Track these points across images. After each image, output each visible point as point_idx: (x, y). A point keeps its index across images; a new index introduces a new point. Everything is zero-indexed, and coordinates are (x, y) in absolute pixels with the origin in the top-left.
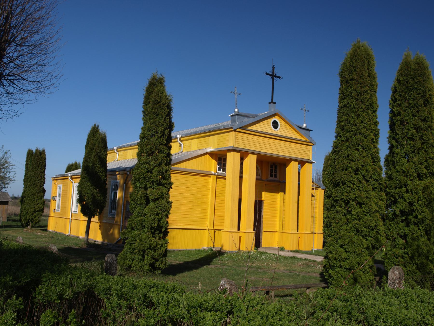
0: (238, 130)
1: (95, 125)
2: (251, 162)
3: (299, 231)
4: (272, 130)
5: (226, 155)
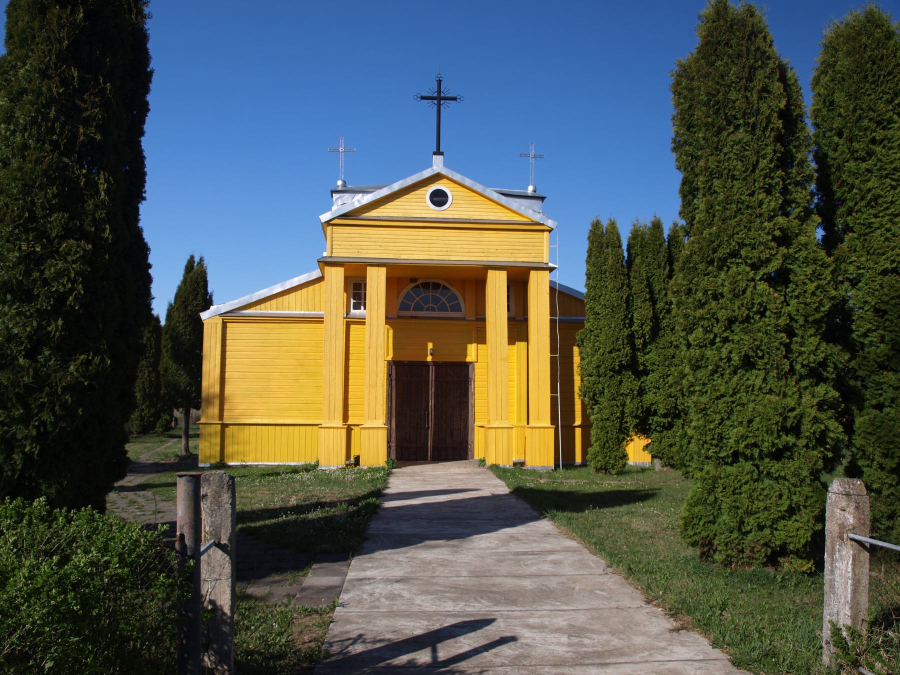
0: (336, 221)
1: (596, 225)
2: (376, 282)
3: (532, 424)
4: (433, 212)
5: (364, 278)
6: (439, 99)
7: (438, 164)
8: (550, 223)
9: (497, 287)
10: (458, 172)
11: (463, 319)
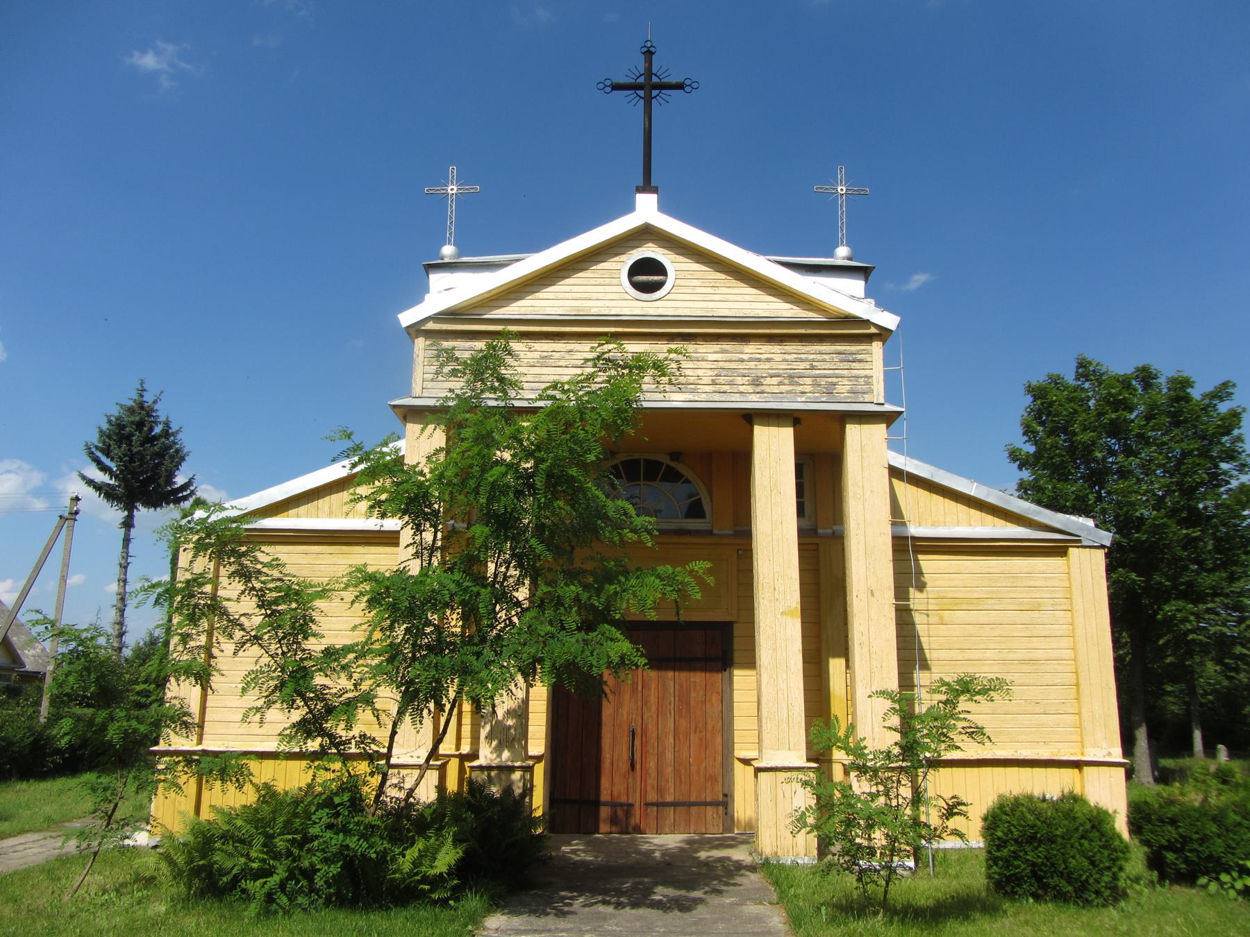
0: (431, 326)
6: (648, 87)
7: (647, 209)
8: (889, 320)
9: (774, 453)
10: (961, 474)
11: (710, 533)
